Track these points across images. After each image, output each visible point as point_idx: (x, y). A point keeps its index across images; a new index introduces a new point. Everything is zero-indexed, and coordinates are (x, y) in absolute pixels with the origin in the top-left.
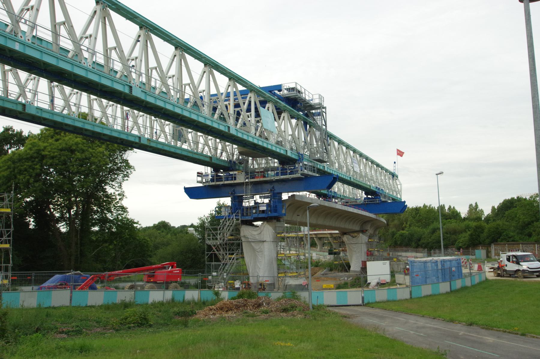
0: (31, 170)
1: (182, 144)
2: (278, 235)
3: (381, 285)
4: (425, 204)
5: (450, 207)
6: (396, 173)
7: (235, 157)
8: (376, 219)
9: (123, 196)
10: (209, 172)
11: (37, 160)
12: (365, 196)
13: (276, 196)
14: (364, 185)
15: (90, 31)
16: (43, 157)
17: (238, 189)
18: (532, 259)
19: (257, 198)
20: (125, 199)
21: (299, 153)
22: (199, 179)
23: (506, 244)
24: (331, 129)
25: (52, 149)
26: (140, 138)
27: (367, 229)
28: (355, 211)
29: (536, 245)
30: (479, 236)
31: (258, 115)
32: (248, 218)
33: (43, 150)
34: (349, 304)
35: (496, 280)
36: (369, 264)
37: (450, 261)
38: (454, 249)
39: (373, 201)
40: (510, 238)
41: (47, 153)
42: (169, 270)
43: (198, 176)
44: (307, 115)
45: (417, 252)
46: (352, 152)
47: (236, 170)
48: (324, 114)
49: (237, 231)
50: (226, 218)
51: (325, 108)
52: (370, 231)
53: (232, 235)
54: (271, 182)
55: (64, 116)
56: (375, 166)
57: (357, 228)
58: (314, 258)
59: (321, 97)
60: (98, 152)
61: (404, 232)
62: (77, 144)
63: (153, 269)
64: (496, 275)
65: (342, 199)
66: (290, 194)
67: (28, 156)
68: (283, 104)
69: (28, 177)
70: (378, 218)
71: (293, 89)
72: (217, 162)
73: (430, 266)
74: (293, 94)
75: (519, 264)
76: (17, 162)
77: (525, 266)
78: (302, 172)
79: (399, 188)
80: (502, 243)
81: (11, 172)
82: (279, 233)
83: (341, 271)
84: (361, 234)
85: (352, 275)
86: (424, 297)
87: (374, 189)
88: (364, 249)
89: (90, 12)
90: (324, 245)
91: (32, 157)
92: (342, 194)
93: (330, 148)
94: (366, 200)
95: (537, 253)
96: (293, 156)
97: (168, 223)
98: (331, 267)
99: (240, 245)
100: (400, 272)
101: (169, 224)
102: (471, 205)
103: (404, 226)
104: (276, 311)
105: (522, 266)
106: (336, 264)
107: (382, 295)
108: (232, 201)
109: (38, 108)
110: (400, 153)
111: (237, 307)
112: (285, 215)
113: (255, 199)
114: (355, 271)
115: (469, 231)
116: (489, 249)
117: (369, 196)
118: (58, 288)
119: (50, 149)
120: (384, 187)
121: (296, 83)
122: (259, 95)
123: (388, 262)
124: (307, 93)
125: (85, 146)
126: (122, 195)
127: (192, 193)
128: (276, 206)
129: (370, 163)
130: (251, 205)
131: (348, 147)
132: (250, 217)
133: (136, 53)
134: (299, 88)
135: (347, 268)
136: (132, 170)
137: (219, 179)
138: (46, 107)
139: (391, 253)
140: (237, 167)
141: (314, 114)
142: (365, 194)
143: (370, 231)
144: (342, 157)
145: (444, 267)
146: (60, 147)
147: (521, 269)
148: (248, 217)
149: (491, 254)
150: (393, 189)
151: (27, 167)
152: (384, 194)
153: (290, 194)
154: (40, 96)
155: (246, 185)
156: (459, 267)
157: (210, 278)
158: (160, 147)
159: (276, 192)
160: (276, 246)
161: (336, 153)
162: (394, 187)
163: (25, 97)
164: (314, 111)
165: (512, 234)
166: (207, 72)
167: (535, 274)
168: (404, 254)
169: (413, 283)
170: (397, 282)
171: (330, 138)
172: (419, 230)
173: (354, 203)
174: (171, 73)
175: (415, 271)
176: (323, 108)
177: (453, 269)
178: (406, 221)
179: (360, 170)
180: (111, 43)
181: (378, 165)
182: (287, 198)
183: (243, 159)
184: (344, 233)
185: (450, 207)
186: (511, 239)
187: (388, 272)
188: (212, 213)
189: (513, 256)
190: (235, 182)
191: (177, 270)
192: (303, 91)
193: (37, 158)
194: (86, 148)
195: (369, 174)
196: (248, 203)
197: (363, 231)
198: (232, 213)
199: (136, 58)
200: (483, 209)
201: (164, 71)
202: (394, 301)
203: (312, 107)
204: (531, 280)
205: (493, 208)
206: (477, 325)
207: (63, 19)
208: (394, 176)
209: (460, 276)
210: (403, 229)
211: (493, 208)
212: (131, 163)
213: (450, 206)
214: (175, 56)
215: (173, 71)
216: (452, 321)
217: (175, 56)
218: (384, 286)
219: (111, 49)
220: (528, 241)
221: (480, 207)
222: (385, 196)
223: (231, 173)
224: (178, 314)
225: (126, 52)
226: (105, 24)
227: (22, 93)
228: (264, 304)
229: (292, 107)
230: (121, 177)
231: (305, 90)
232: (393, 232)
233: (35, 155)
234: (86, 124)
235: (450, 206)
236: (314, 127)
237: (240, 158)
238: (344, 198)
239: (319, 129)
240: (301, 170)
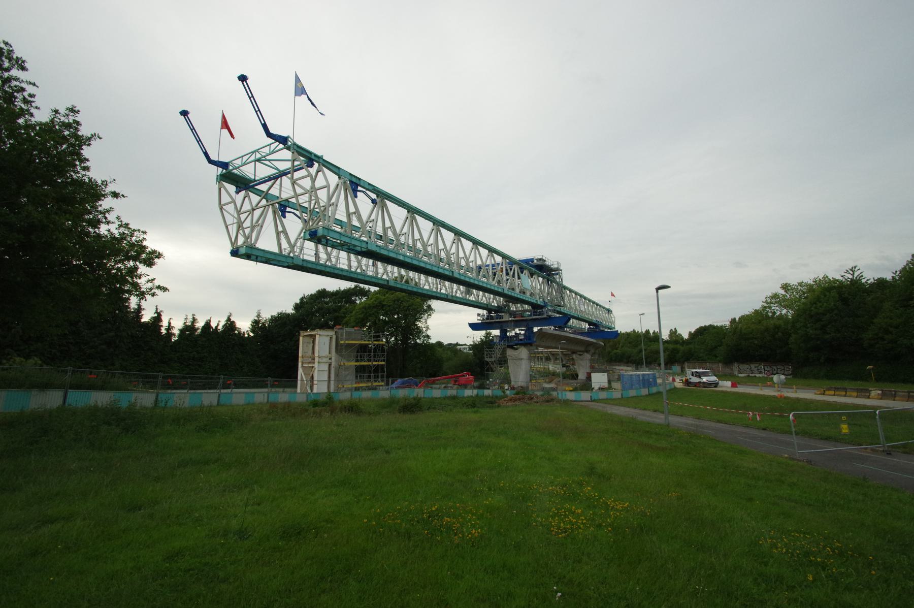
0: (376, 314)
2: (532, 355)
3: (601, 389)
5: (654, 331)
6: (611, 309)
10: (485, 313)
13: (529, 330)
15: (373, 217)
16: (383, 306)
19: (517, 331)
22: (479, 318)
23: (707, 363)
24: (565, 283)
25: (389, 300)
26: (447, 295)
31: (519, 278)
32: (511, 344)
33: (383, 301)
36: (593, 375)
38: (656, 365)
44: (549, 275)
45: (628, 367)
46: (579, 297)
47: (503, 312)
51: (561, 270)
52: (592, 351)
54: (526, 320)
55: (358, 274)
58: (550, 369)
59: (558, 263)
61: (618, 351)
63: (457, 376)
65: (571, 328)
66: (539, 328)
68: (534, 269)
69: (375, 318)
71: (540, 259)
72: (491, 307)
74: (540, 263)
79: (613, 320)
82: (532, 354)
83: (572, 379)
84: (586, 354)
87: (595, 322)
88: (588, 364)
89: (404, 218)
90: (556, 359)
91: (377, 306)
96: (541, 304)
98: (565, 377)
99: (506, 362)
102: (671, 330)
103: (617, 346)
107: (603, 395)
108: (500, 332)
109: (303, 260)
111: (520, 399)
112: (536, 342)
114: (582, 380)
120: (598, 318)
122: (519, 265)
123: (606, 374)
124: (549, 261)
126: (428, 328)
127: (474, 327)
133: (405, 230)
134: (544, 258)
137: (492, 318)
138: (345, 267)
140: (503, 310)
141: (554, 274)
143: (592, 351)
144: (572, 301)
153: (539, 328)
154: (341, 260)
162: (610, 319)
163: (331, 261)
166: (456, 239)
168: (617, 368)
170: (613, 387)
174: (452, 252)
177: (651, 380)
180: (388, 224)
183: (506, 305)
184: (574, 353)
185: (654, 331)
190: (503, 320)
191: (471, 377)
192: (547, 260)
196: (511, 334)
197: (587, 351)
198: (501, 341)
199: (405, 233)
201: (425, 241)
203: (552, 270)
207: (354, 210)
208: (609, 311)
209: (655, 384)
210: (616, 349)
212: (433, 306)
214: (433, 230)
215: (431, 241)
217: (433, 230)
219: (388, 228)
221: (679, 331)
223: (500, 314)
225: (398, 231)
226: (383, 211)
227: (292, 251)
233: (379, 304)
239: (557, 283)
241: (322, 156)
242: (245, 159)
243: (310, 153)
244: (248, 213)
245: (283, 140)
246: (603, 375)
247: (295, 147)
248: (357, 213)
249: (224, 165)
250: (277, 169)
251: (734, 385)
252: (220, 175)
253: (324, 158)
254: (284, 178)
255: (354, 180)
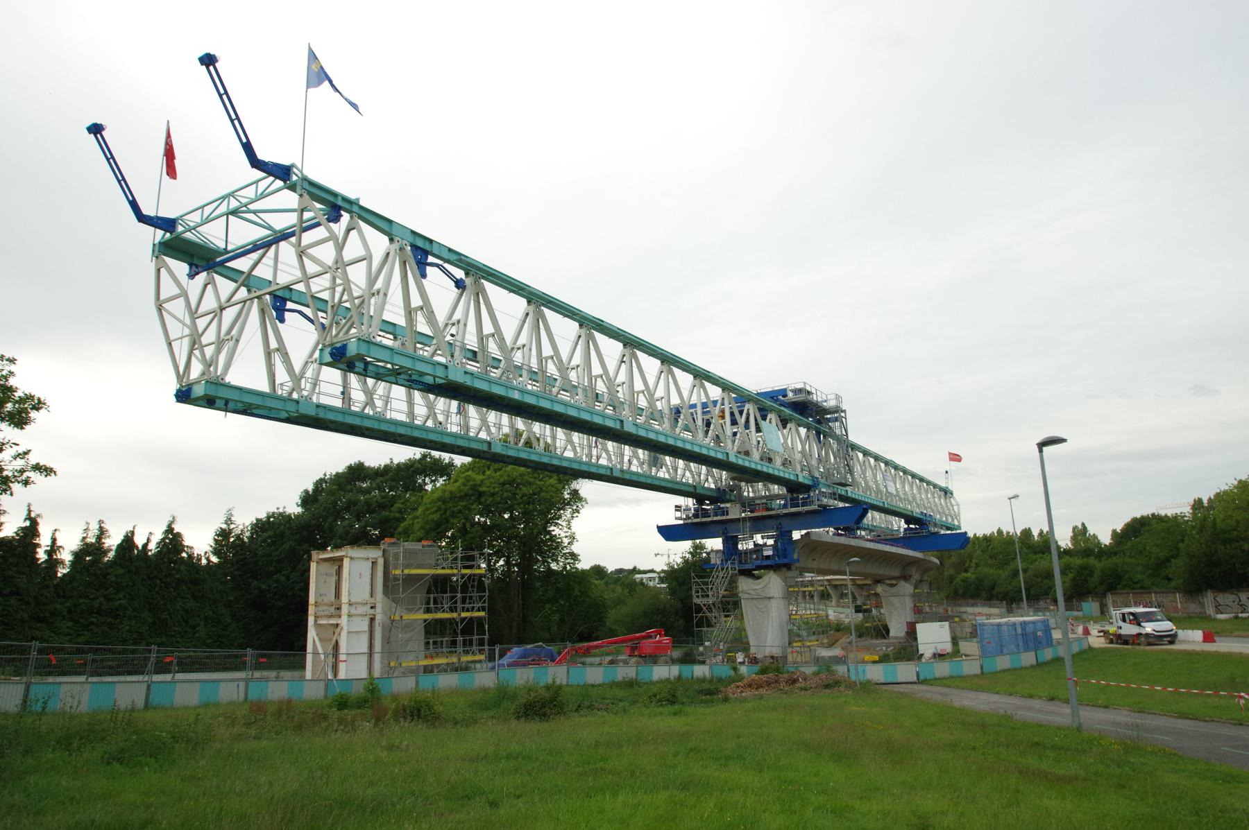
0: (467, 512)
1: (658, 470)
3: (939, 656)
4: (999, 528)
6: (950, 488)
7: (724, 483)
8: (925, 560)
9: (574, 538)
11: (473, 498)
12: (906, 526)
14: (903, 512)
17: (730, 527)
18: (1159, 618)
19: (758, 538)
20: (575, 543)
21: (812, 477)
22: (678, 514)
23: (1129, 593)
24: (854, 438)
25: (491, 483)
26: (611, 469)
27: (910, 574)
28: (893, 549)
29: (1177, 594)
30: (1087, 581)
32: (746, 567)
33: (480, 485)
34: (899, 681)
35: (1105, 648)
36: (919, 627)
37: (1034, 623)
38: (1048, 601)
39: (918, 533)
40: (1137, 583)
41: (485, 489)
42: (657, 639)
43: (676, 510)
44: (819, 422)
45: (990, 606)
46: (882, 465)
48: (844, 419)
49: (732, 584)
50: (717, 568)
51: (844, 411)
53: (726, 590)
56: (918, 481)
57: (896, 573)
58: (830, 617)
59: (838, 397)
60: (549, 486)
61: (969, 574)
62: (521, 475)
63: (637, 638)
64: (1108, 641)
66: (804, 532)
67: (462, 494)
68: (787, 411)
70: (927, 558)
73: (1006, 630)
74: (801, 397)
75: (1139, 624)
76: (449, 502)
77: (1149, 628)
78: (820, 503)
80: (1124, 591)
81: (441, 515)
82: (790, 586)
83: (876, 637)
85: (893, 643)
86: (1001, 671)
87: (919, 516)
88: (909, 603)
89: (573, 337)
90: (842, 596)
91: (466, 495)
92: (870, 523)
93: (853, 463)
94: (908, 532)
95: (1179, 607)
96: (807, 482)
97: (605, 567)
98: (862, 632)
99: (737, 604)
100: (966, 638)
101: (605, 569)
102: (1075, 528)
103: (967, 565)
104: (816, 688)
105: (1144, 627)
106: (867, 628)
107: (943, 669)
110: (955, 458)
111: (768, 684)
112: (798, 560)
113: (754, 539)
114: (896, 638)
115: (1071, 573)
116: (1104, 601)
117: (911, 526)
118: (531, 664)
119: (488, 484)
120: (933, 511)
121: (805, 383)
122: (756, 403)
123: (947, 624)
124: (819, 393)
125: (530, 477)
126: (573, 538)
127: (669, 533)
128: (785, 550)
129: (910, 477)
130: (750, 547)
131: (877, 458)
132: (750, 565)
134: (808, 388)
135: (884, 632)
136: (583, 503)
137: (705, 513)
139: (950, 609)
141: (829, 420)
142: (906, 523)
144: (869, 473)
145: (1025, 630)
146: (501, 481)
147: (1143, 632)
148: (746, 565)
149: (1107, 609)
150: (947, 512)
151: (462, 508)
152: (934, 521)
153: (804, 532)
155: (743, 521)
156: (1047, 630)
157: (701, 649)
158: (634, 478)
159: (783, 530)
160: (787, 604)
161: (861, 468)
164: (829, 416)
165: (1139, 577)
167: (1165, 639)
168: (970, 610)
169: (984, 654)
170: (962, 652)
171: (852, 449)
172: (991, 571)
173: (889, 537)
175: (985, 636)
176: (843, 411)
178: (970, 557)
179: (896, 489)
181: (922, 480)
182: (799, 537)
184: (878, 581)
186: (1139, 585)
187: (949, 639)
188: (684, 555)
189: (1131, 614)
190: (728, 517)
191: (666, 640)
192: (814, 391)
193: (473, 495)
194: (533, 480)
195: (909, 493)
196: (745, 545)
197: (906, 578)
198: (727, 561)
200: (1096, 534)
202: (959, 677)
204: (1172, 649)
205: (1114, 532)
206: (1060, 700)
207: (421, 303)
208: (946, 492)
209: (1050, 642)
210: (966, 571)
211: (1114, 532)
212: (582, 493)
213: (1041, 530)
216: (1031, 696)
217: (580, 337)
218: (944, 657)
220: (1167, 588)
221: (1091, 530)
222: (935, 525)
223: (722, 506)
224: (701, 692)
226: (479, 302)
228: (800, 680)
229: (801, 414)
230: (568, 512)
231: (816, 390)
232: (951, 575)
233: (471, 492)
234: (553, 459)
235: (1041, 530)
236: (831, 436)
237: (731, 483)
238: (873, 528)
240: (818, 500)
241: (358, 199)
242: (208, 210)
243: (335, 195)
244: (213, 314)
245: (282, 172)
246: (941, 627)
247: (306, 185)
248: (426, 308)
249: (167, 224)
250: (269, 228)
251: (1208, 638)
252: (160, 243)
253: (361, 203)
254: (283, 244)
255: (420, 243)
